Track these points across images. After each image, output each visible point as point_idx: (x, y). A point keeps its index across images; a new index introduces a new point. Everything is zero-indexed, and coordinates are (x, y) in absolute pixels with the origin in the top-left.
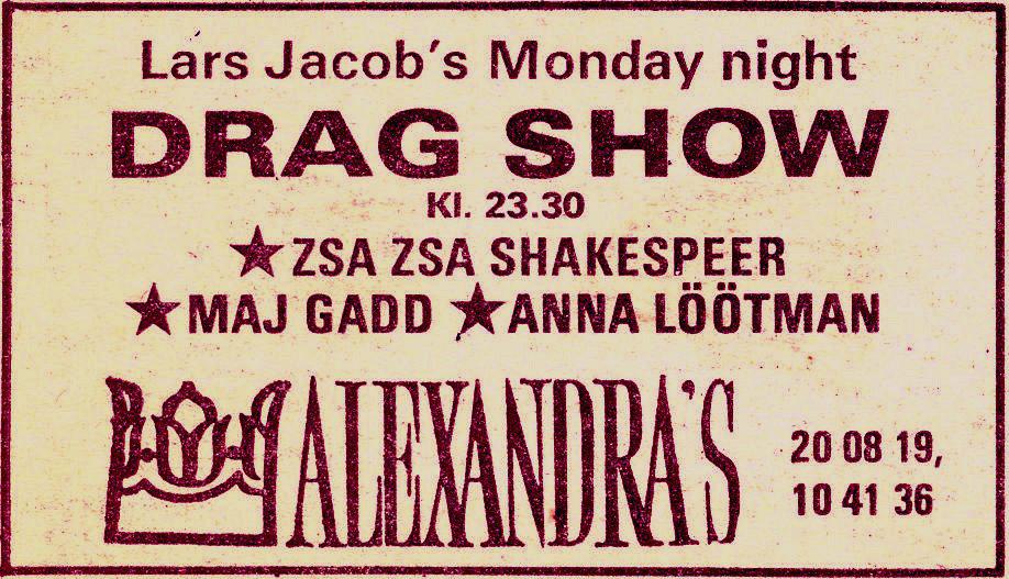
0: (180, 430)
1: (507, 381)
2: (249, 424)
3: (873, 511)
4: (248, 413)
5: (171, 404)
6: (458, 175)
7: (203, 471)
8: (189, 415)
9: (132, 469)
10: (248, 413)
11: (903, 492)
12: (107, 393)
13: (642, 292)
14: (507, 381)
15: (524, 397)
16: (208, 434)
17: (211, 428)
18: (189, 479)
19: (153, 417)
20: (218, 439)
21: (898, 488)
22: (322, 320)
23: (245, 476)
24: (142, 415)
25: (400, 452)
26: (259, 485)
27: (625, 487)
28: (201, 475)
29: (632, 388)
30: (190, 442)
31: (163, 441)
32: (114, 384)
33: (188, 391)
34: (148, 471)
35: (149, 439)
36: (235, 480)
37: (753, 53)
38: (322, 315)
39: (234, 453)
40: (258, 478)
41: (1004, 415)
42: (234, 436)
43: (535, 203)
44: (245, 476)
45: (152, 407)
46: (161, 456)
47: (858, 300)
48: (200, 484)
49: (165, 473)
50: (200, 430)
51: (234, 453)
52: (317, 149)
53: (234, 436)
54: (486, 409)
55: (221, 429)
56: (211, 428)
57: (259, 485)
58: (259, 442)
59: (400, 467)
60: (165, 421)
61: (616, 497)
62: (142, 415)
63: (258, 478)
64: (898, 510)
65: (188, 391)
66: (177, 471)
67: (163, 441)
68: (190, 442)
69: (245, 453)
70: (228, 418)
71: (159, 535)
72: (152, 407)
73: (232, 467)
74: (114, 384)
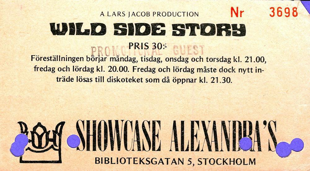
0: (37, 134)
1: (175, 122)
2: (55, 132)
4: (55, 130)
5: (35, 128)
7: (44, 144)
8: (40, 131)
10: (55, 130)
11: (272, 10)
14: (175, 122)
15: (80, 124)
17: (45, 134)
18: (40, 146)
19: (31, 131)
21: (271, 8)
23: (54, 146)
24: (28, 131)
25: (195, 134)
26: (58, 148)
27: (150, 142)
28: (43, 146)
29: (250, 123)
30: (40, 137)
31: (33, 137)
32: (20, 123)
33: (39, 125)
34: (30, 145)
35: (30, 137)
36: (52, 147)
37: (203, 68)
39: (51, 140)
40: (57, 146)
41: (244, 133)
42: (51, 136)
43: (130, 69)
44: (54, 146)
45: (30, 129)
46: (33, 141)
48: (43, 148)
49: (34, 145)
50: (42, 135)
51: (51, 140)
53: (51, 136)
55: (48, 133)
56: (45, 134)
57: (58, 148)
58: (58, 137)
59: (156, 137)
60: (33, 132)
61: (153, 141)
62: (28, 131)
63: (57, 146)
64: (270, 15)
65: (39, 125)
66: (37, 144)
67: (33, 137)
68: (40, 137)
69: (54, 140)
70: (50, 131)
71: (183, 128)
72: (30, 129)
73: (51, 143)
74: (20, 123)
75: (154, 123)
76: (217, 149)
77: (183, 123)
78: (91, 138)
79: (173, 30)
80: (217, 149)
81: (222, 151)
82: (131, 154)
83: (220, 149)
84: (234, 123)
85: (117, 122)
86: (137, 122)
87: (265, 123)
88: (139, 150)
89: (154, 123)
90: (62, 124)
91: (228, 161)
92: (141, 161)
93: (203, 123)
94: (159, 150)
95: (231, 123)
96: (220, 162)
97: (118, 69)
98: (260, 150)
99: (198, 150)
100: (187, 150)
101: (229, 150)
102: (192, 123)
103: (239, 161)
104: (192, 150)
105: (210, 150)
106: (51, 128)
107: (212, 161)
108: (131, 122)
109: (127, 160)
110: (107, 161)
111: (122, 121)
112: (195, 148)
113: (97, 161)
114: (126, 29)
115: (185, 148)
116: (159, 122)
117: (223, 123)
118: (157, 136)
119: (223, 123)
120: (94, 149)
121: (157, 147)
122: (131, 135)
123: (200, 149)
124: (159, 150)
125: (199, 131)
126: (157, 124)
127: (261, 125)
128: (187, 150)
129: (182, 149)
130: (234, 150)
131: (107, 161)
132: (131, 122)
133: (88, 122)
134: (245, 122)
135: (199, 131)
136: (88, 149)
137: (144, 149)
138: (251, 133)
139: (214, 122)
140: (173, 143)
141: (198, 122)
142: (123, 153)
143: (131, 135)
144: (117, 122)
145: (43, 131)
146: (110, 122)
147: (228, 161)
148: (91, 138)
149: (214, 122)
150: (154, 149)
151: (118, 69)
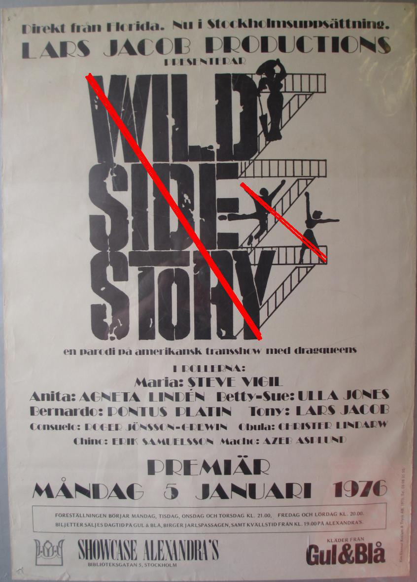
3: (146, 542)
6: (281, 140)
8: (48, 546)
9: (39, 554)
12: (34, 542)
13: (120, 403)
16: (51, 548)
20: (53, 549)
22: (314, 558)
25: (134, 549)
26: (60, 557)
30: (48, 550)
32: (36, 540)
33: (47, 541)
34: (42, 554)
38: (314, 556)
39: (55, 551)
45: (42, 544)
47: (361, 538)
52: (194, 244)
53: (55, 549)
54: (176, 543)
55: (53, 547)
58: (60, 549)
59: (134, 551)
68: (48, 550)
69: (58, 551)
72: (42, 544)
74: (36, 540)
75: (132, 541)
76: (176, 559)
77: (152, 542)
78: (89, 551)
79: (173, 76)
80: (176, 559)
81: (180, 560)
82: (115, 562)
83: (178, 559)
84: (188, 542)
85: (106, 541)
86: (120, 541)
87: (210, 541)
88: (122, 559)
89: (132, 541)
90: (62, 541)
91: (161, 565)
92: (113, 565)
93: (167, 542)
94: (136, 559)
95: (186, 542)
96: (157, 565)
97: (356, 514)
98: (206, 559)
99: (163, 559)
100: (156, 559)
101: (184, 559)
102: (159, 542)
103: (167, 565)
104: (159, 559)
105: (171, 559)
106: (55, 544)
107: (152, 565)
108: (116, 541)
109: (106, 564)
110: (95, 565)
111: (110, 540)
112: (161, 558)
113: (90, 565)
114: (216, 248)
115: (154, 558)
116: (136, 541)
117: (181, 542)
118: (162, 550)
119: (181, 542)
120: (91, 558)
121: (134, 558)
122: (116, 549)
123: (165, 559)
124: (136, 559)
125: (164, 547)
126: (134, 543)
127: (207, 544)
128: (156, 559)
129: (152, 559)
130: (188, 559)
131: (95, 565)
132: (116, 541)
133: (86, 541)
134: (196, 541)
135: (164, 547)
136: (87, 558)
137: (125, 559)
138: (200, 548)
139: (174, 541)
140: (146, 555)
141: (163, 541)
142: (111, 560)
143: (116, 549)
144: (106, 541)
145: (50, 546)
146: (101, 541)
147: (161, 565)
148: (89, 551)
149: (174, 541)
150: (132, 559)
151: (356, 514)
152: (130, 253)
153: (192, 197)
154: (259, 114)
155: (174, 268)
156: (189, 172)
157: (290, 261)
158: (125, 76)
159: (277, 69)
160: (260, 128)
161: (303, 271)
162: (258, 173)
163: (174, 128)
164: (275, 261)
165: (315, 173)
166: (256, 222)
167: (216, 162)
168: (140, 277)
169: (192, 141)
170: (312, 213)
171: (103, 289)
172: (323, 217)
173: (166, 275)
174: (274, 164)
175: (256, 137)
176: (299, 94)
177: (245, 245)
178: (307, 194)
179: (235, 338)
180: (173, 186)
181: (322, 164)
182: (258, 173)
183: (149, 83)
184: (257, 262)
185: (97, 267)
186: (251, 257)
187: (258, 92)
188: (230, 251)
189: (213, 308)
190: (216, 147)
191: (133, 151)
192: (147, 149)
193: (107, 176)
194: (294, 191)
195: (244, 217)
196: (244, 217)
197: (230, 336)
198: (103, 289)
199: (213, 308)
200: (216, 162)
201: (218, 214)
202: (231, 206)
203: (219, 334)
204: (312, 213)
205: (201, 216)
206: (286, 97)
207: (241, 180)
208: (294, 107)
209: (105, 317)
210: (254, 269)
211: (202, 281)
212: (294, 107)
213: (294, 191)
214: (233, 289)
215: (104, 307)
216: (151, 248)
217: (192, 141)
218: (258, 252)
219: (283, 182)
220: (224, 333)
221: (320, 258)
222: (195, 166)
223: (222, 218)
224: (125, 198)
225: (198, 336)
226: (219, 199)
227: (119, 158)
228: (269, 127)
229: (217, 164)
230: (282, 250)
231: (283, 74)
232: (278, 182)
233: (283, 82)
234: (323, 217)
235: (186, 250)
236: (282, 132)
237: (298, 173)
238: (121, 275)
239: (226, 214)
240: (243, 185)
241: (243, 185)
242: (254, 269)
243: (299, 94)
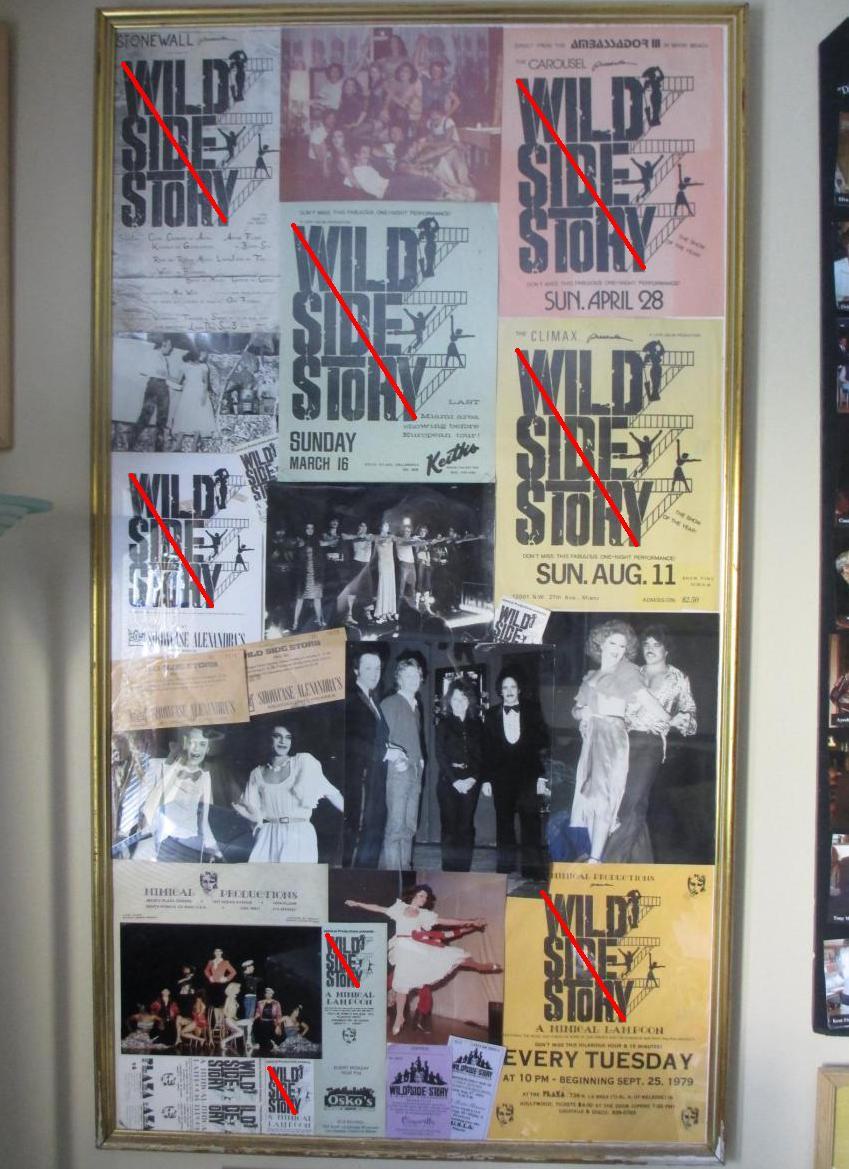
152: (549, 210)
153: (594, 168)
154: (644, 106)
155: (581, 219)
156: (593, 943)
157: (667, 213)
158: (544, 351)
159: (658, 348)
160: (645, 117)
161: (674, 497)
162: (643, 150)
163: (581, 117)
164: (653, 489)
165: (684, 425)
166: (640, 460)
167: (611, 416)
168: (557, 227)
169: (594, 400)
170: (681, 454)
171: (525, 508)
172: (689, 458)
173: (575, 226)
174: (655, 143)
175: (641, 398)
176: (673, 366)
177: (634, 202)
178: (678, 441)
179: (621, 545)
180: (580, 433)
181: (690, 80)
182: (643, 150)
183: (561, 92)
184: (640, 489)
185: (524, 220)
186: (636, 486)
187: (642, 91)
188: (621, 481)
189: (604, 1008)
190: (612, 405)
191: (551, 134)
192: (561, 132)
193: (530, 153)
194: (669, 438)
195: (633, 182)
196: (633, 182)
197: (623, 269)
198: (525, 508)
199: (604, 1008)
200: (612, 142)
201: (612, 454)
202: (622, 449)
203: (615, 268)
204: (681, 454)
205: (600, 455)
206: (664, 369)
207: (629, 430)
208: (670, 101)
209: (526, 528)
210: (638, 495)
211: (602, 229)
212: (670, 101)
213: (669, 438)
214: (625, 796)
215: (526, 456)
216: (562, 478)
217: (594, 400)
218: (641, 482)
219: (661, 432)
220: (614, 541)
221: (690, 212)
222: (596, 145)
223: (615, 457)
224: (545, 169)
225: (595, 544)
226: (614, 444)
227: (540, 139)
228: (651, 391)
229: (615, 145)
230: (659, 482)
231: (662, 352)
232: (657, 431)
233: (662, 358)
234: (689, 458)
235: (590, 206)
236: (660, 395)
237: (672, 425)
238: (542, 225)
239: (618, 454)
240: (631, 434)
241: (631, 434)
242: (638, 495)
243: (673, 366)
